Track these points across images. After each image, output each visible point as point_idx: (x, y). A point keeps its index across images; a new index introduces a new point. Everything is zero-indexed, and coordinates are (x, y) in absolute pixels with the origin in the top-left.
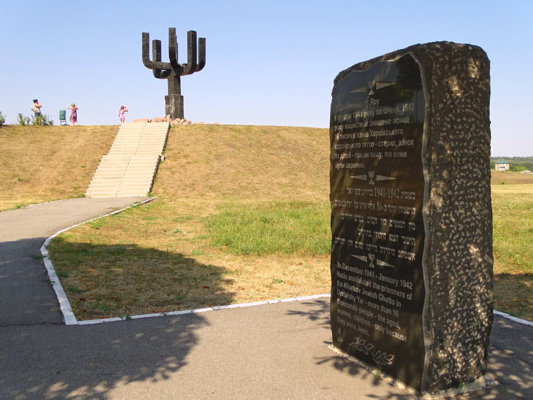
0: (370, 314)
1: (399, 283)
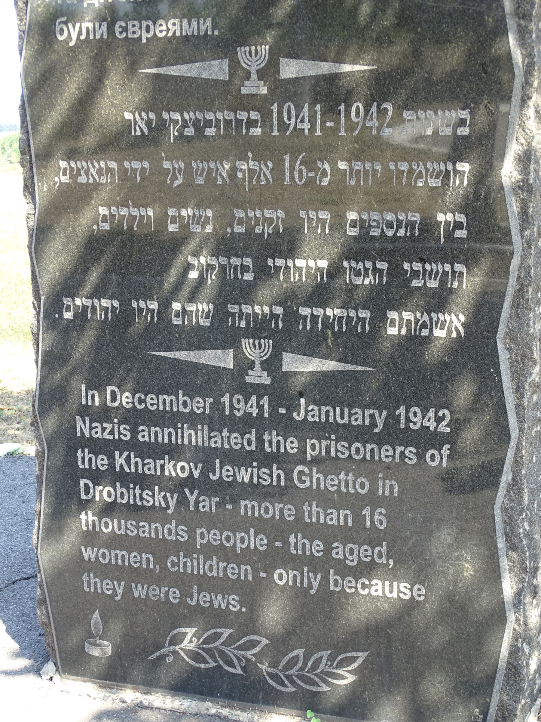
0: (257, 542)
1: (393, 418)
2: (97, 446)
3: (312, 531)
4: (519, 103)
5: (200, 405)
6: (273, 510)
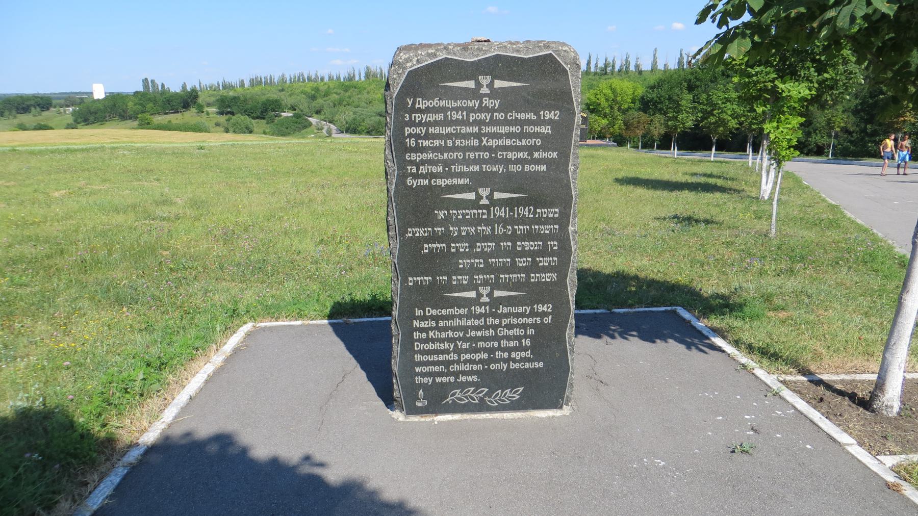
0: (485, 356)
1: (532, 309)
2: (421, 330)
3: (504, 350)
4: (681, 211)
5: (462, 311)
6: (490, 345)
